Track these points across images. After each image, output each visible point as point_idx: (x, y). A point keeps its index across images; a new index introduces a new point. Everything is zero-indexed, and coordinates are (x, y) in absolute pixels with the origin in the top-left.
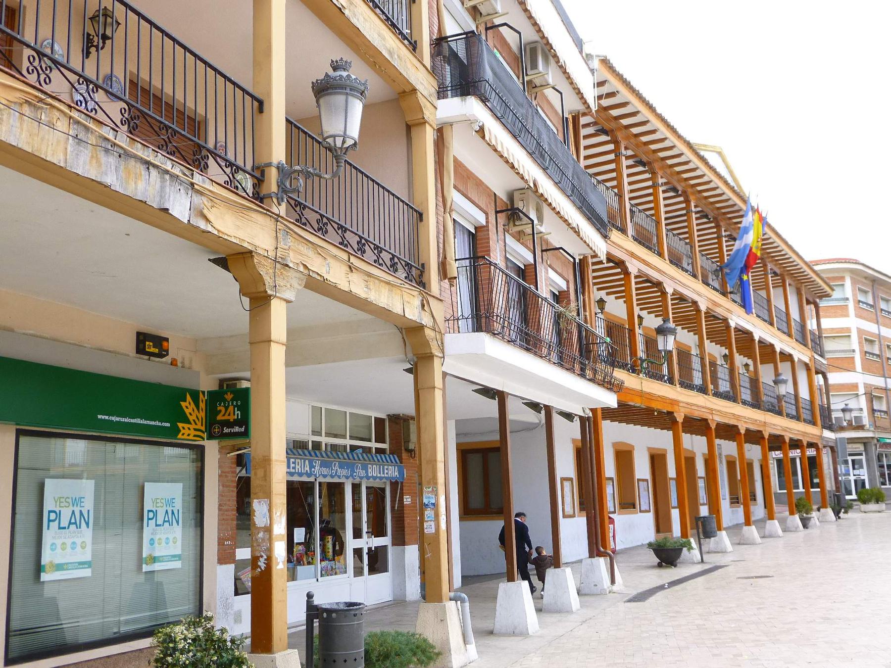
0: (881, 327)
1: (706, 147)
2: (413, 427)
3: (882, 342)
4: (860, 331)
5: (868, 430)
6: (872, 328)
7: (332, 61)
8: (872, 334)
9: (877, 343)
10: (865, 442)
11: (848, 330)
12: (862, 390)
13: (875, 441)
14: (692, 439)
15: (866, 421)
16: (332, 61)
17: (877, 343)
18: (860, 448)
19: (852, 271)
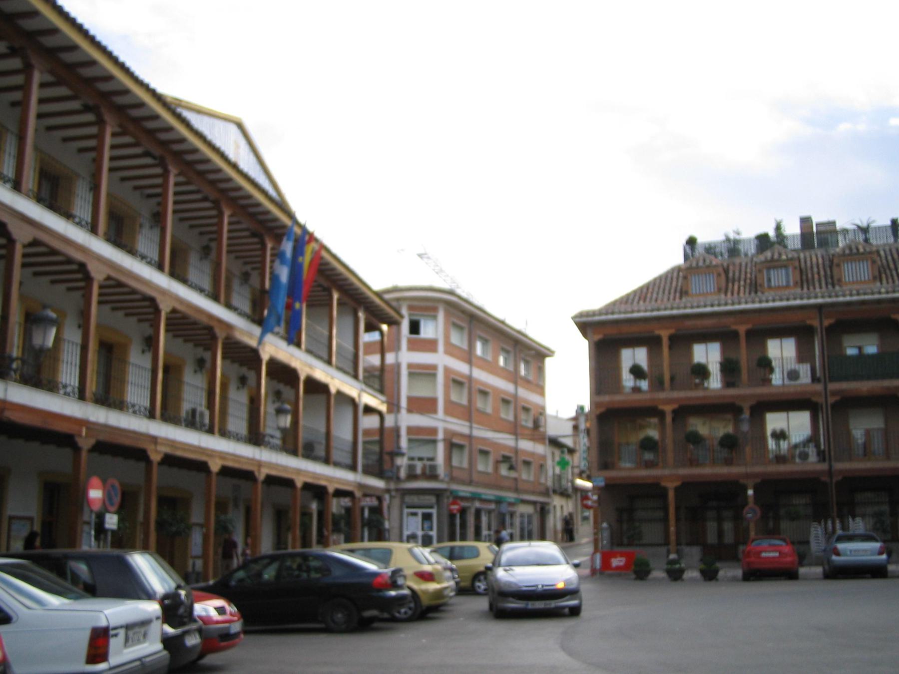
0: (475, 425)
1: (179, 103)
2: (324, 254)
3: (473, 385)
4: (447, 370)
5: (442, 481)
6: (462, 367)
7: (691, 242)
8: (462, 435)
9: (467, 385)
10: (438, 494)
11: (434, 367)
12: (441, 436)
13: (448, 494)
14: (261, 457)
15: (441, 471)
16: (691, 242)
17: (467, 385)
18: (432, 499)
19: (448, 303)
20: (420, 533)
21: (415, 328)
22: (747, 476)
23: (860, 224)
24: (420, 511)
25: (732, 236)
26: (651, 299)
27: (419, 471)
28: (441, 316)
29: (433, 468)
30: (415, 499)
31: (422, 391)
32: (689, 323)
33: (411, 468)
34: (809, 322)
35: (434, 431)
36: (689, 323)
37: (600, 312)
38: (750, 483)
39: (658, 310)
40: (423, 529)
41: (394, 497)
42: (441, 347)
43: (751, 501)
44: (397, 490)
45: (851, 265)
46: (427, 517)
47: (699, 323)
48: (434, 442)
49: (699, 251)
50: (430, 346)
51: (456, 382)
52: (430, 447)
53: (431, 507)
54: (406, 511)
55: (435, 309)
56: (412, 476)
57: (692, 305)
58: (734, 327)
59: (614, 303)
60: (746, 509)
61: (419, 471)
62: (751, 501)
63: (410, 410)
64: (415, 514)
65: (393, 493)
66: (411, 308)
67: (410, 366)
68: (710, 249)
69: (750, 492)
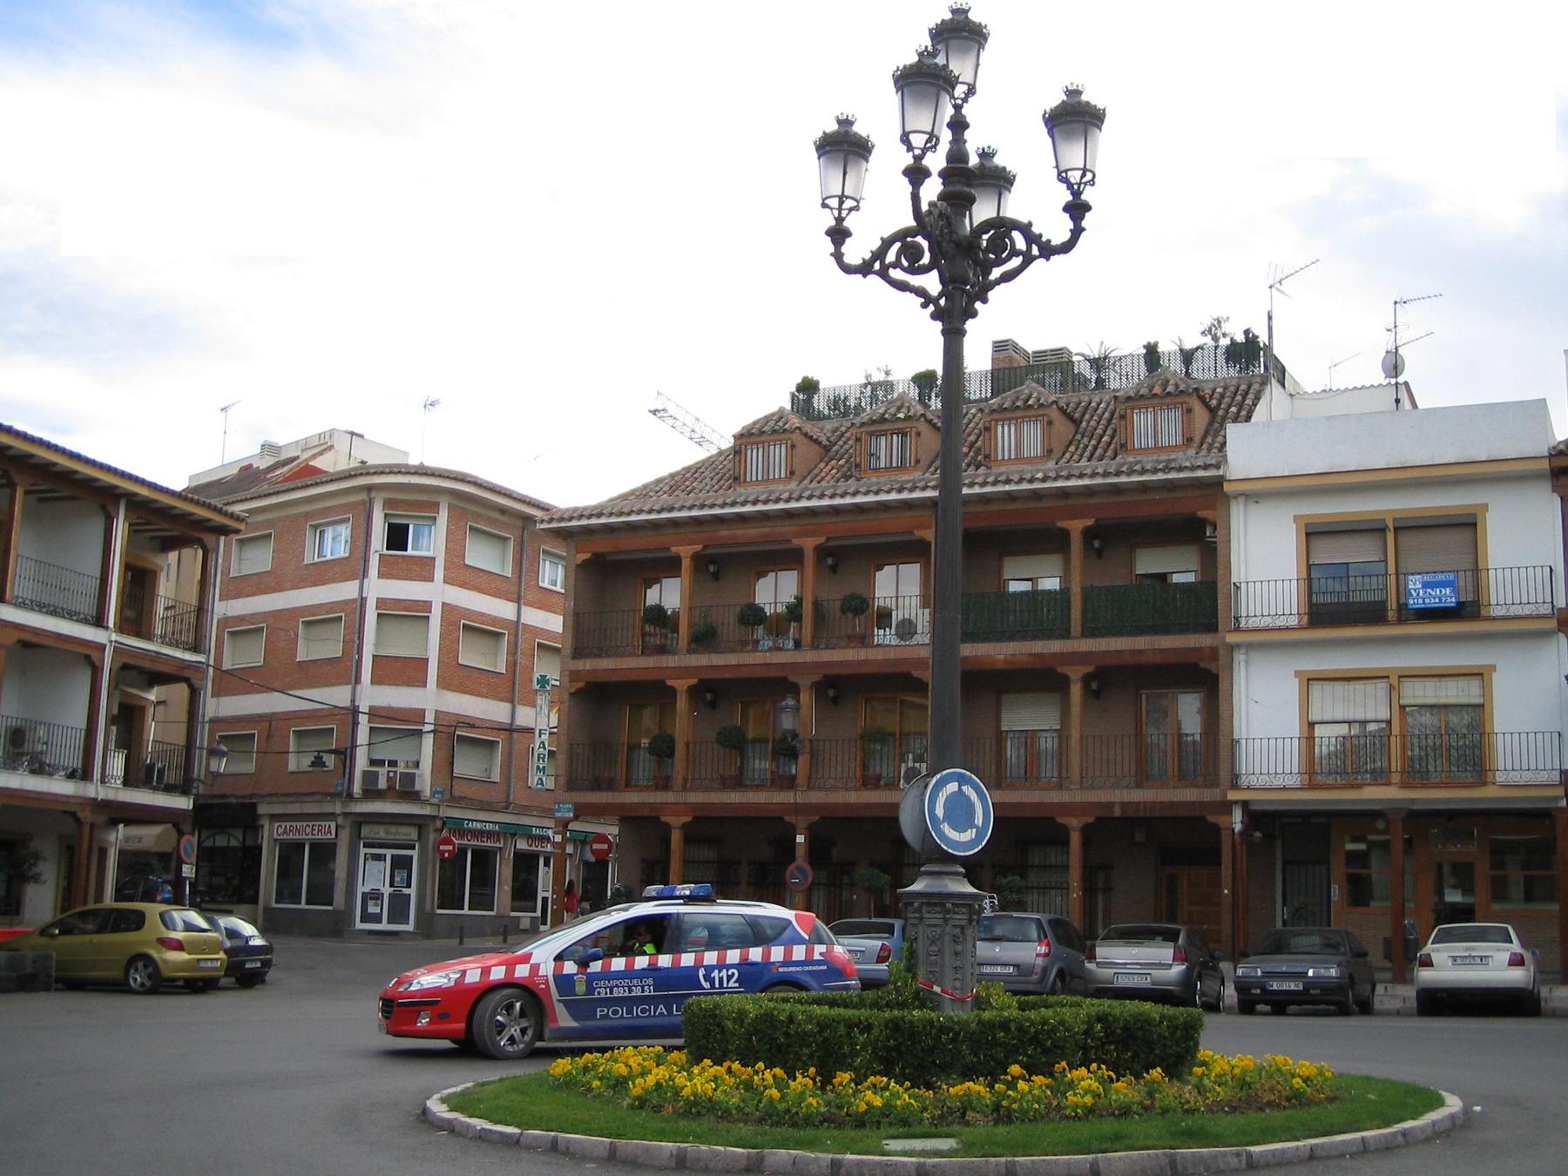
5: (425, 802)
7: (808, 387)
10: (420, 823)
12: (430, 718)
15: (425, 779)
18: (413, 833)
20: (387, 890)
21: (397, 537)
22: (797, 809)
23: (1088, 352)
24: (389, 853)
25: (878, 377)
26: (1092, 455)
27: (382, 784)
28: (443, 517)
29: (409, 779)
30: (380, 832)
31: (401, 646)
32: (724, 533)
33: (370, 778)
34: (919, 534)
35: (419, 715)
36: (724, 533)
37: (598, 512)
38: (801, 822)
39: (671, 509)
40: (392, 885)
41: (342, 827)
42: (439, 573)
43: (801, 853)
44: (346, 815)
45: (1003, 427)
46: (401, 864)
47: (742, 532)
48: (419, 734)
49: (820, 403)
50: (422, 569)
51: (462, 625)
52: (412, 741)
53: (413, 848)
54: (363, 851)
55: (435, 506)
56: (371, 793)
57: (1105, 471)
58: (796, 542)
59: (624, 497)
60: (792, 867)
61: (382, 784)
62: (801, 853)
63: (377, 680)
64: (380, 858)
65: (340, 820)
66: (388, 504)
67: (381, 602)
68: (838, 403)
69: (800, 839)
